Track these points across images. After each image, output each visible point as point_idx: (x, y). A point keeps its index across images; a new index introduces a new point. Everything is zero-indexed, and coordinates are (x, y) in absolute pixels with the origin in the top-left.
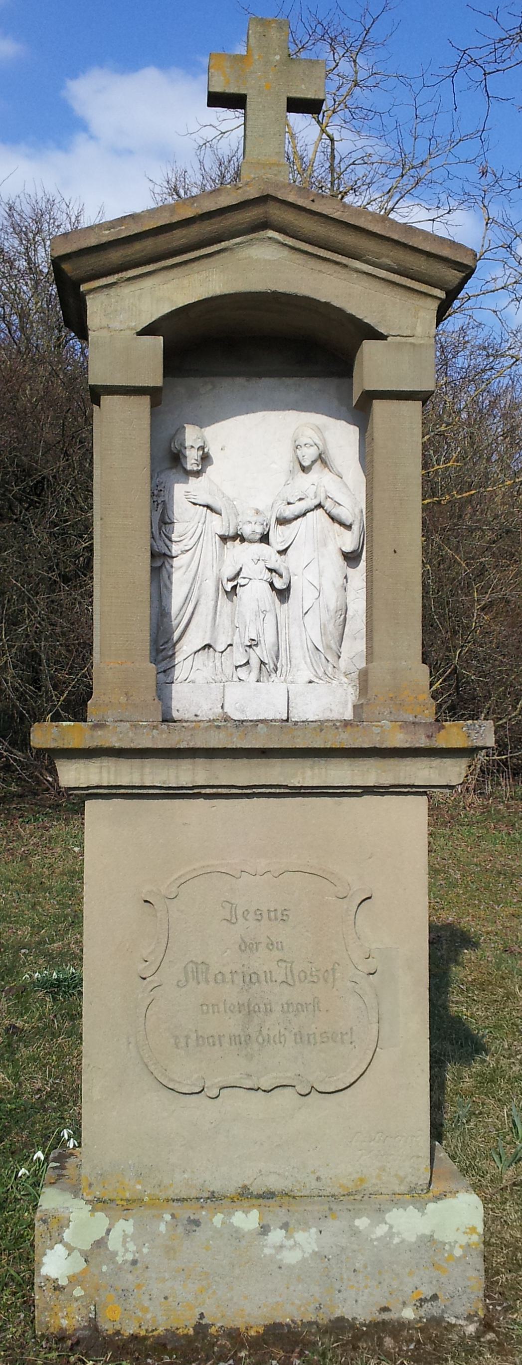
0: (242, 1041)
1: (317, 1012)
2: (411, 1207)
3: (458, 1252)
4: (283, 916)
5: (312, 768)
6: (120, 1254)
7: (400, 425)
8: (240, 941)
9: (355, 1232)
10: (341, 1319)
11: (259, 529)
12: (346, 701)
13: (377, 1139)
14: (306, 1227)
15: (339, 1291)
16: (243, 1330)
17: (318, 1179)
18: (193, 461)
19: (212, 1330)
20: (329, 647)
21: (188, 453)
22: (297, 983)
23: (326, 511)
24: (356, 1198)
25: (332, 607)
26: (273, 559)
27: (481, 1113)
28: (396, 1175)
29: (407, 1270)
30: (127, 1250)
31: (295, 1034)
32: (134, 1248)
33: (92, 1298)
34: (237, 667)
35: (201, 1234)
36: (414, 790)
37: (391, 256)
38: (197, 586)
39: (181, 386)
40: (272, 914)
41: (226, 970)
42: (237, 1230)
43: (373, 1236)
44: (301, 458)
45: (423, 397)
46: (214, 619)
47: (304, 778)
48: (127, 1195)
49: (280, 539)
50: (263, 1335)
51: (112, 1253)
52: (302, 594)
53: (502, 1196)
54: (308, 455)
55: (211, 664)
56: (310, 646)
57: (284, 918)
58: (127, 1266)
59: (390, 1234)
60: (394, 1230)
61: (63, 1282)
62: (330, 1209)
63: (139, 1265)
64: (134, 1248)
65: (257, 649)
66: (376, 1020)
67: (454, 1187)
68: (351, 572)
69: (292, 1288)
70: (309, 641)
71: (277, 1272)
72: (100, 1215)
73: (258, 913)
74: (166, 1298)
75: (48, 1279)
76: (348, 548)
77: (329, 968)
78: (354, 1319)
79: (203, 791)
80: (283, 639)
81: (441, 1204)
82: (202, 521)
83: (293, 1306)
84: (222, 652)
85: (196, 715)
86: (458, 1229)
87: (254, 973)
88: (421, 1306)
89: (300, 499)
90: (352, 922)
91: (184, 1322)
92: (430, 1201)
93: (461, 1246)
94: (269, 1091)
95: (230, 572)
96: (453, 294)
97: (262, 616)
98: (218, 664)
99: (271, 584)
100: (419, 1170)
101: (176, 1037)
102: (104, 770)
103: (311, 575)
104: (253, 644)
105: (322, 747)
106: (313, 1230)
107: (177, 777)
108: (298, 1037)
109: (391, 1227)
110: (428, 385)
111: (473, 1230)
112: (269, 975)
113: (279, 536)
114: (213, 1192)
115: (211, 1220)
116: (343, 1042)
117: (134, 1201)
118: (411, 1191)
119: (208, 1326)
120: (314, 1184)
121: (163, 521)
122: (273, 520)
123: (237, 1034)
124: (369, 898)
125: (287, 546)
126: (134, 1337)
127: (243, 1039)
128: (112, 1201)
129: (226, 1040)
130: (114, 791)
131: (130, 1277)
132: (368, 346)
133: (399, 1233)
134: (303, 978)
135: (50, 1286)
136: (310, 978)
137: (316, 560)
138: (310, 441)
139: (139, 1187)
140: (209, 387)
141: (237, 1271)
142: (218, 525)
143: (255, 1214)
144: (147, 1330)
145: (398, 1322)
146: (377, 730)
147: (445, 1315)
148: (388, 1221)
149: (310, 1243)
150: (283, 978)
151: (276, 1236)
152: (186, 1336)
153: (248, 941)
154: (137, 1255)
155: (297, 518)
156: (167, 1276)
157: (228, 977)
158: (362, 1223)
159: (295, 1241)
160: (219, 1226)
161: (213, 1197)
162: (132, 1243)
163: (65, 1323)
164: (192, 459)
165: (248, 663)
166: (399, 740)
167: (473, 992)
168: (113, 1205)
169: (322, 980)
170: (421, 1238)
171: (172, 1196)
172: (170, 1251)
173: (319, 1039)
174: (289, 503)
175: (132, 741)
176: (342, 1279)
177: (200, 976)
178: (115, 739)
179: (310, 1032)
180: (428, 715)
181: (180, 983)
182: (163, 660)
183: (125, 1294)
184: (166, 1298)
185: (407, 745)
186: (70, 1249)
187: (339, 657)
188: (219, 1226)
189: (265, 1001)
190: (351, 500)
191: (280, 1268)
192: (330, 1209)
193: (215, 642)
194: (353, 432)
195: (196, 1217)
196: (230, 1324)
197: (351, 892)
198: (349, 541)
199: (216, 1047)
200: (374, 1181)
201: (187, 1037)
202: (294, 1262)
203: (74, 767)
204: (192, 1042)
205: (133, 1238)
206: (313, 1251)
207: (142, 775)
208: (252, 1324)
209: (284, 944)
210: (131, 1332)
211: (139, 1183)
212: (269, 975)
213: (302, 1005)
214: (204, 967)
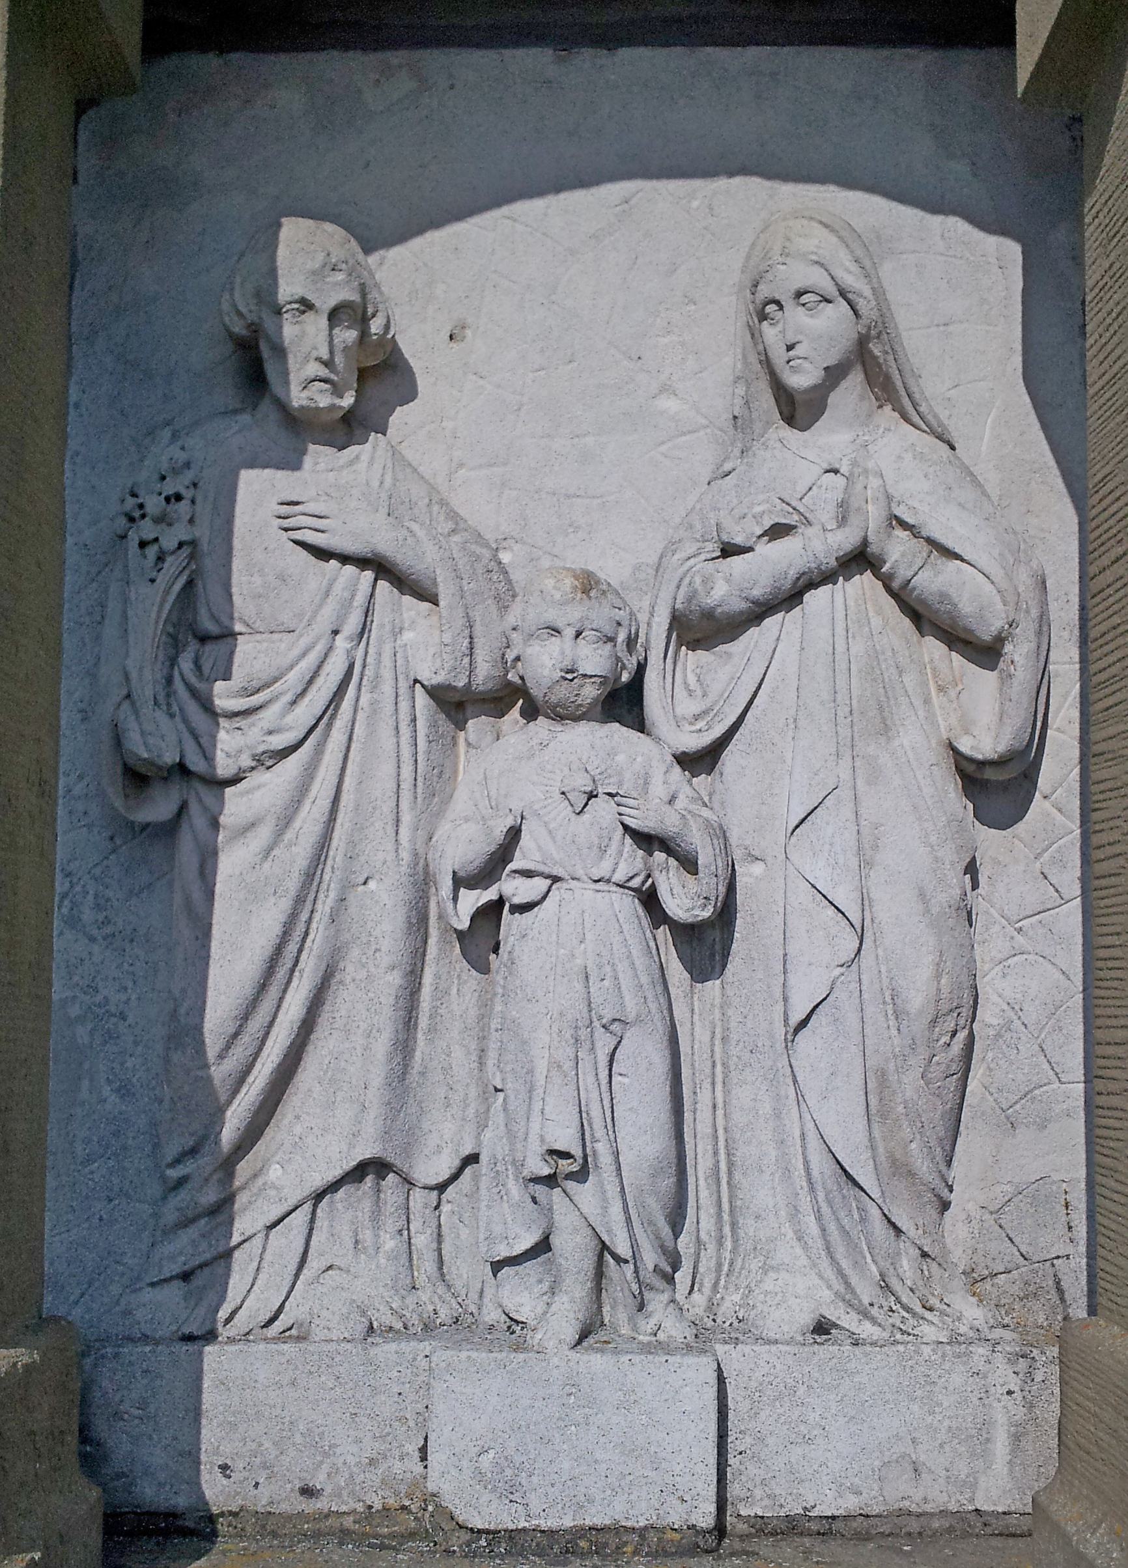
11: (594, 660)
12: (986, 1425)
18: (315, 369)
20: (900, 1169)
21: (289, 331)
23: (886, 582)
25: (917, 999)
26: (658, 790)
34: (497, 1266)
38: (324, 907)
44: (778, 355)
46: (404, 1046)
49: (687, 707)
52: (790, 938)
54: (814, 338)
55: (390, 1243)
56: (820, 1164)
65: (585, 1193)
68: (988, 839)
70: (812, 1135)
76: (984, 743)
80: (704, 1128)
82: (352, 624)
84: (441, 1187)
85: (308, 1492)
89: (777, 531)
95: (461, 843)
97: (604, 1044)
98: (422, 1240)
99: (650, 900)
103: (823, 860)
104: (565, 1170)
113: (686, 695)
122: (662, 621)
125: (718, 731)
137: (845, 793)
138: (818, 279)
140: (404, 84)
142: (422, 643)
155: (761, 611)
165: (543, 1246)
174: (729, 551)
182: (186, 1223)
187: (945, 1206)
193: (408, 1149)
194: (1002, 258)
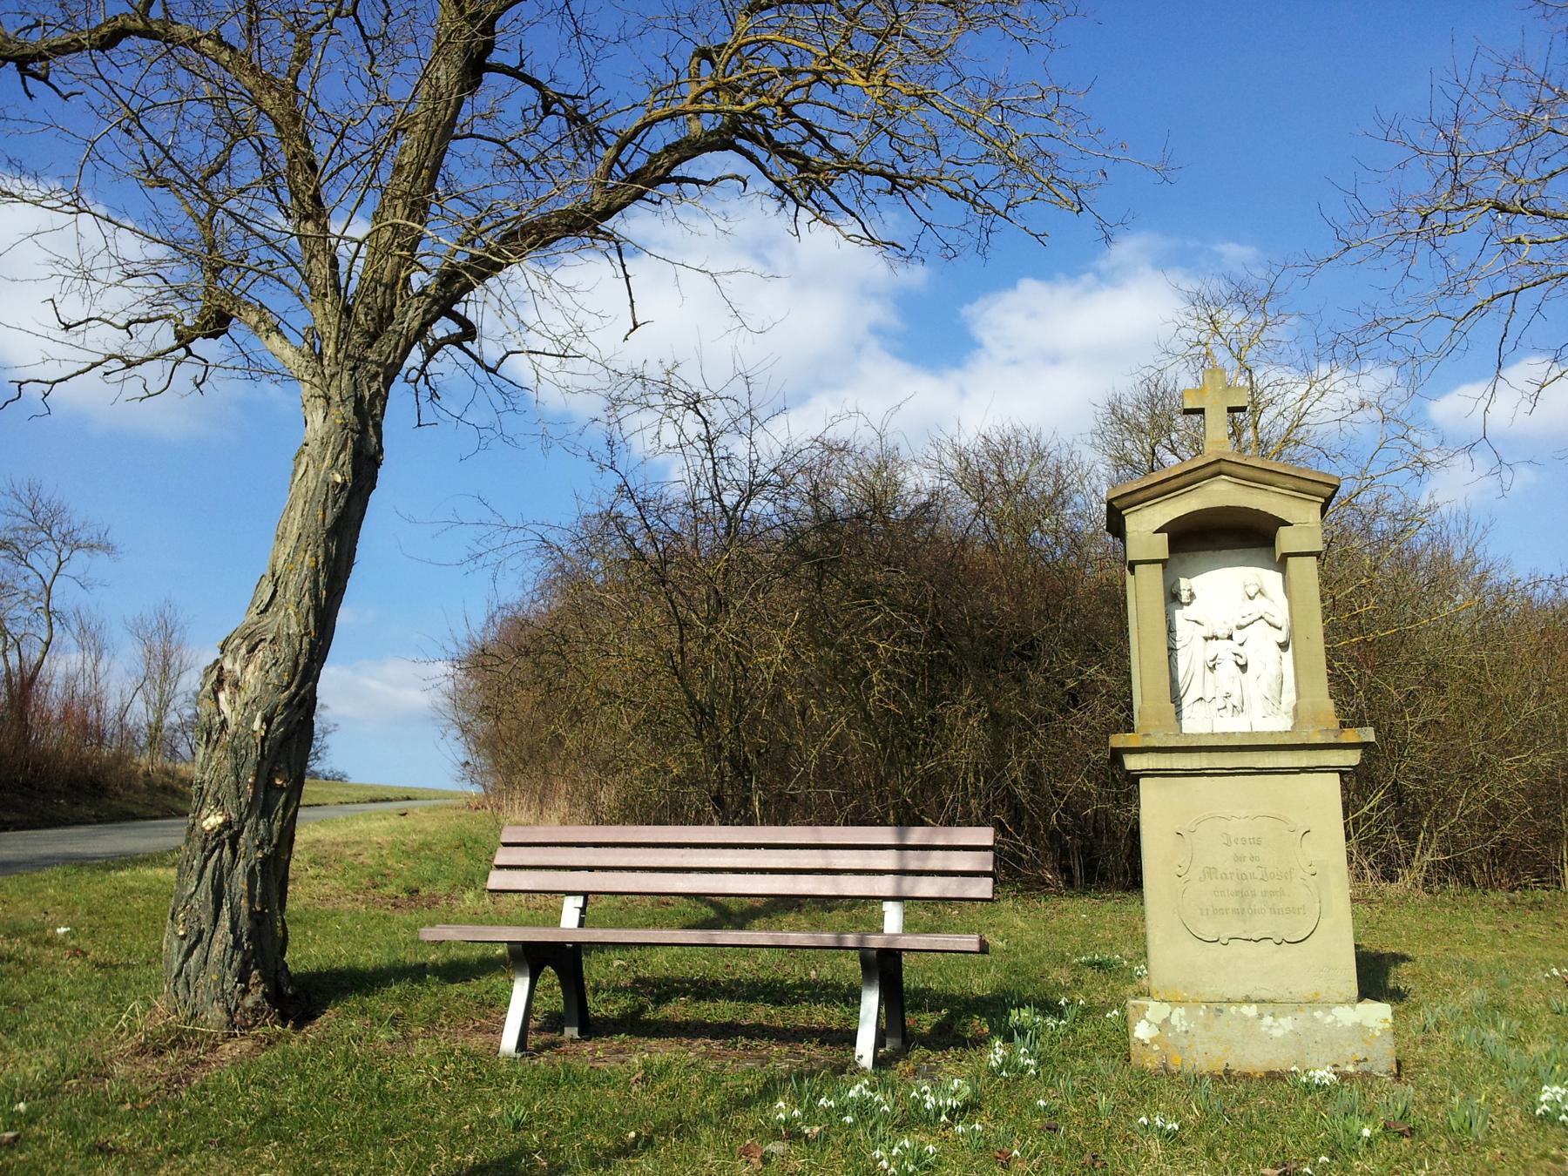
0: (1240, 912)
3: (1378, 1033)
7: (1306, 572)
9: (1314, 1020)
11: (1227, 633)
14: (1285, 1016)
37: (1291, 483)
39: (1175, 560)
45: (1317, 555)
54: (1252, 591)
59: (1336, 1021)
96: (1328, 500)
110: (1320, 547)
121: (1171, 631)
132: (1282, 529)
151: (1268, 1020)
158: (1318, 1014)
164: (1185, 597)
166: (1319, 739)
180: (1336, 725)
190: (1281, 614)
198: (1282, 637)
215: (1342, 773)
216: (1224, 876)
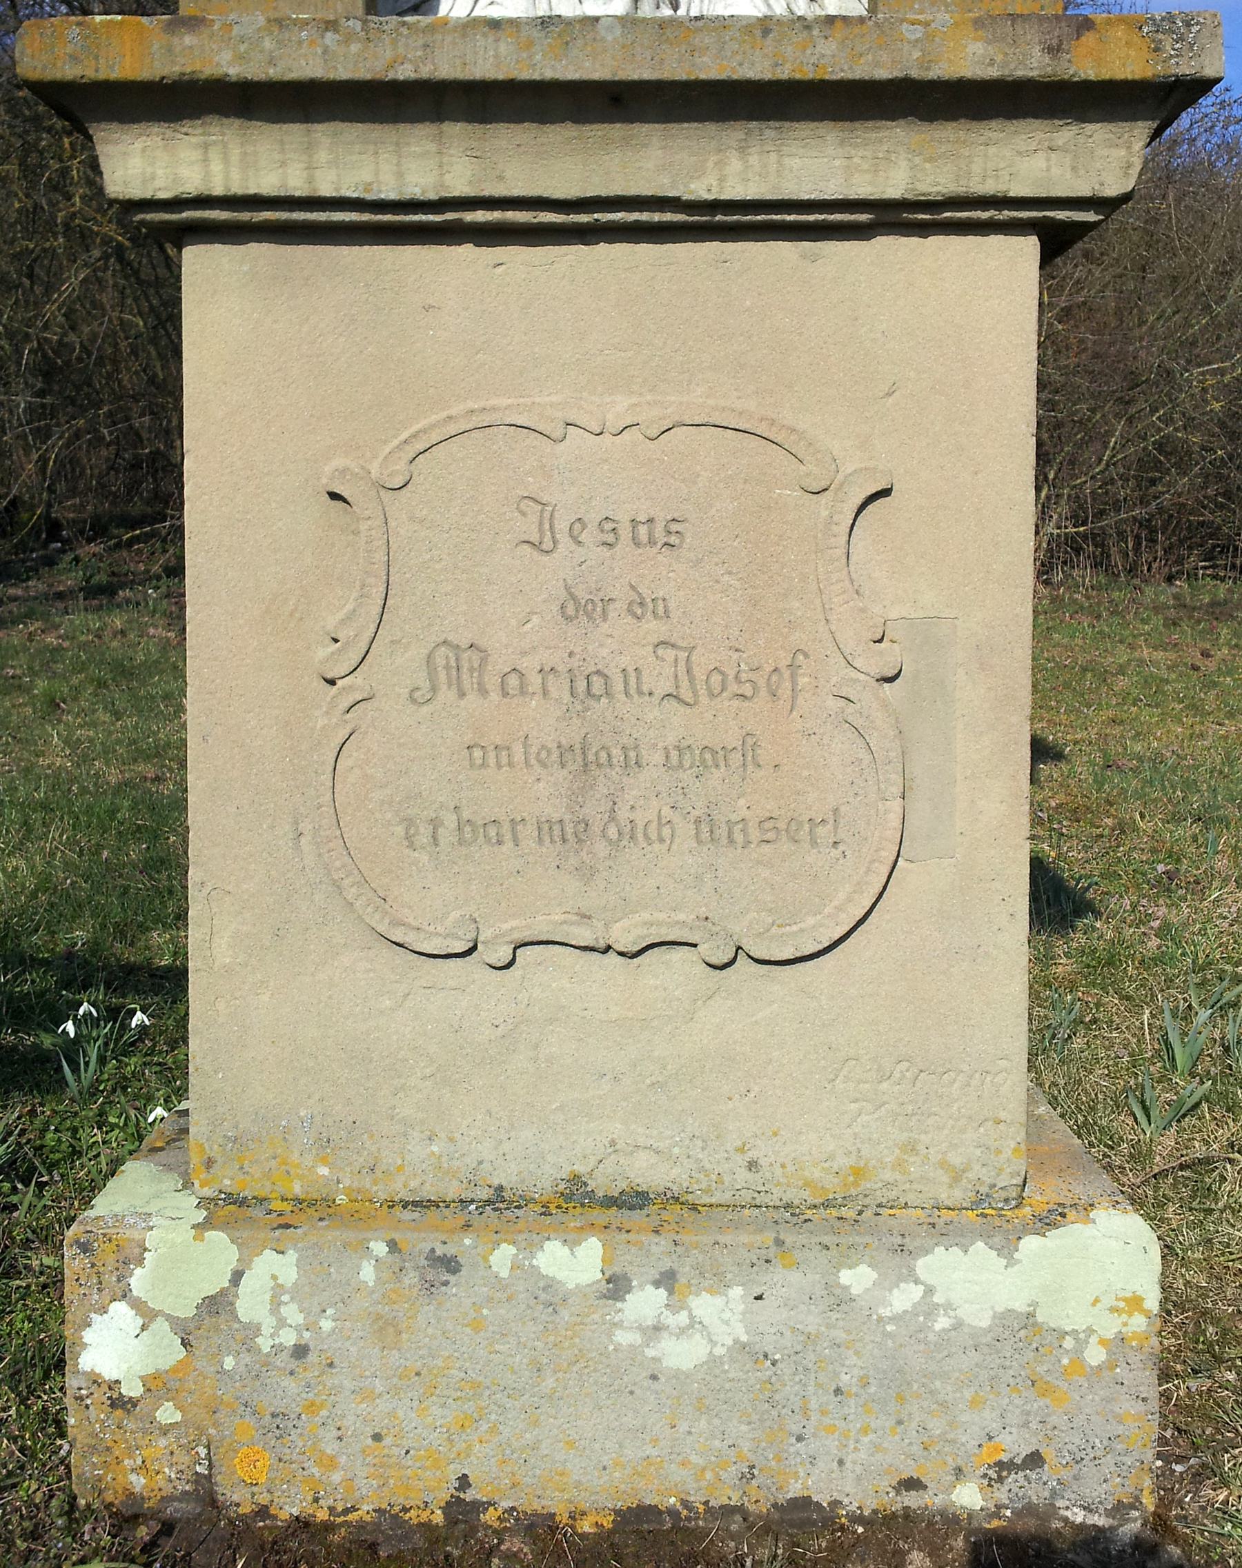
0: (568, 834)
1: (750, 768)
2: (980, 1244)
3: (1095, 1355)
4: (667, 536)
5: (743, 150)
6: (266, 1330)
8: (563, 595)
9: (840, 1300)
10: (803, 1503)
13: (897, 1075)
14: (720, 1285)
15: (800, 1439)
16: (563, 1518)
17: (752, 1165)
19: (490, 1517)
22: (704, 700)
24: (842, 1217)
27: (1094, 1021)
28: (943, 1164)
29: (968, 1394)
30: (282, 1323)
31: (698, 821)
32: (299, 1319)
33: (201, 1430)
35: (459, 1291)
36: (1007, 214)
40: (643, 530)
41: (529, 664)
42: (550, 1285)
43: (885, 1312)
47: (722, 180)
48: (297, 1189)
50: (611, 1532)
51: (246, 1326)
53: (1156, 1189)
57: (673, 539)
58: (283, 1360)
59: (928, 1308)
60: (937, 1298)
61: (131, 1389)
62: (779, 1243)
63: (312, 1358)
64: (299, 1319)
66: (896, 790)
67: (1080, 1190)
69: (683, 1427)
71: (655, 1385)
72: (216, 1236)
73: (609, 526)
74: (377, 1437)
75: (96, 1380)
77: (783, 664)
78: (835, 1504)
79: (470, 217)
81: (1056, 1239)
83: (686, 1466)
86: (1096, 1301)
87: (598, 672)
88: (1000, 1480)
90: (841, 552)
91: (424, 1495)
92: (1025, 1230)
93: (1102, 1342)
94: (634, 956)
100: (998, 1152)
101: (409, 822)
102: (214, 155)
105: (768, 76)
106: (736, 1292)
107: (400, 175)
108: (705, 828)
109: (930, 1291)
111: (1135, 1303)
112: (633, 680)
114: (500, 1188)
115: (486, 1259)
116: (814, 843)
117: (313, 1203)
118: (979, 1201)
119: (479, 1507)
120: (743, 1176)
123: (556, 817)
124: (885, 493)
126: (302, 1524)
127: (569, 830)
128: (262, 1200)
129: (528, 832)
130: (245, 216)
131: (290, 1384)
133: (948, 1306)
134: (717, 688)
135: (100, 1395)
136: (733, 688)
139: (324, 1171)
141: (550, 1382)
143: (592, 1250)
144: (332, 1509)
145: (942, 1513)
146: (912, 33)
147: (1060, 1503)
148: (922, 1277)
149: (727, 1323)
150: (668, 687)
151: (645, 1302)
152: (426, 1526)
153: (582, 594)
154: (307, 1335)
156: (379, 1386)
157: (535, 681)
158: (857, 1278)
159: (691, 1317)
160: (505, 1273)
161: (499, 1200)
162: (294, 1307)
163: (138, 1482)
166: (972, 59)
167: (1060, 822)
168: (258, 1213)
169: (763, 692)
170: (1005, 1318)
171: (404, 1195)
172: (386, 1329)
173: (755, 834)
175: (271, 62)
176: (805, 1410)
177: (465, 676)
178: (226, 56)
179: (734, 818)
181: (417, 694)
183: (279, 1424)
184: (377, 1437)
185: (993, 73)
186: (147, 1315)
188: (505, 1273)
189: (625, 740)
191: (654, 1377)
192: (779, 1243)
195: (450, 1250)
196: (531, 1504)
197: (840, 477)
199: (504, 848)
200: (888, 1176)
201: (435, 823)
202: (686, 1364)
203: (138, 145)
204: (447, 836)
205: (296, 1292)
206: (736, 1341)
207: (310, 168)
208: (584, 1506)
209: (672, 605)
210: (295, 1512)
211: (324, 1161)
212: (633, 680)
213: (714, 753)
214: (476, 657)
215: (1056, 241)
216: (514, 684)
